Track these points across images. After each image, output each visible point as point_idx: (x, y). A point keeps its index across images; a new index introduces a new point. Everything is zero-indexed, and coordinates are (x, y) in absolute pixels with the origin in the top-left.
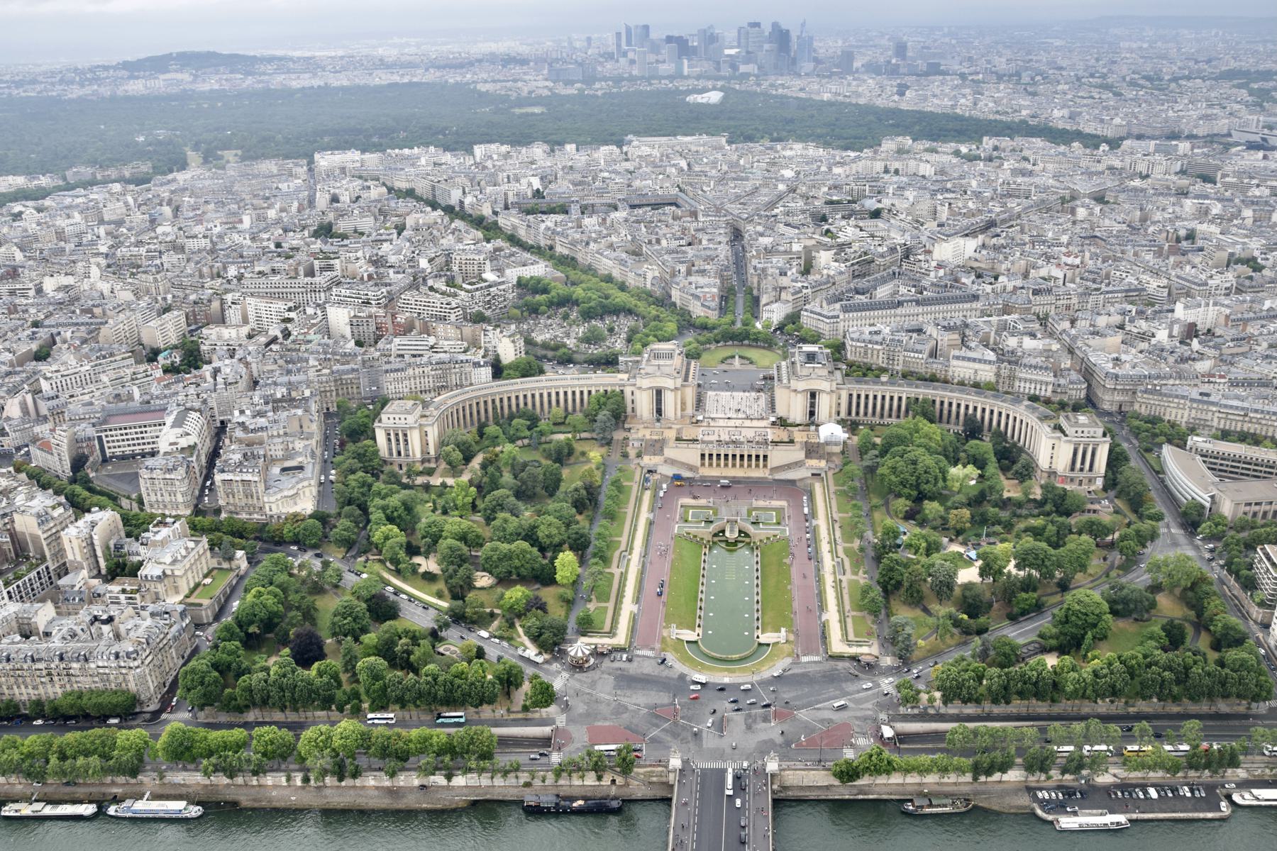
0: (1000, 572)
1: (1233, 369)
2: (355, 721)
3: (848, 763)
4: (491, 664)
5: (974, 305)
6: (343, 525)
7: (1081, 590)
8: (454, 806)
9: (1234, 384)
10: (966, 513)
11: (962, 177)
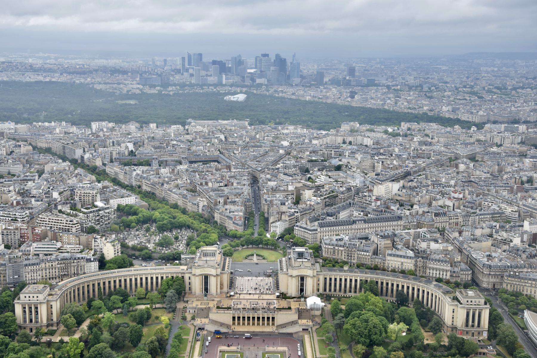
5: (399, 223)
11: (389, 146)
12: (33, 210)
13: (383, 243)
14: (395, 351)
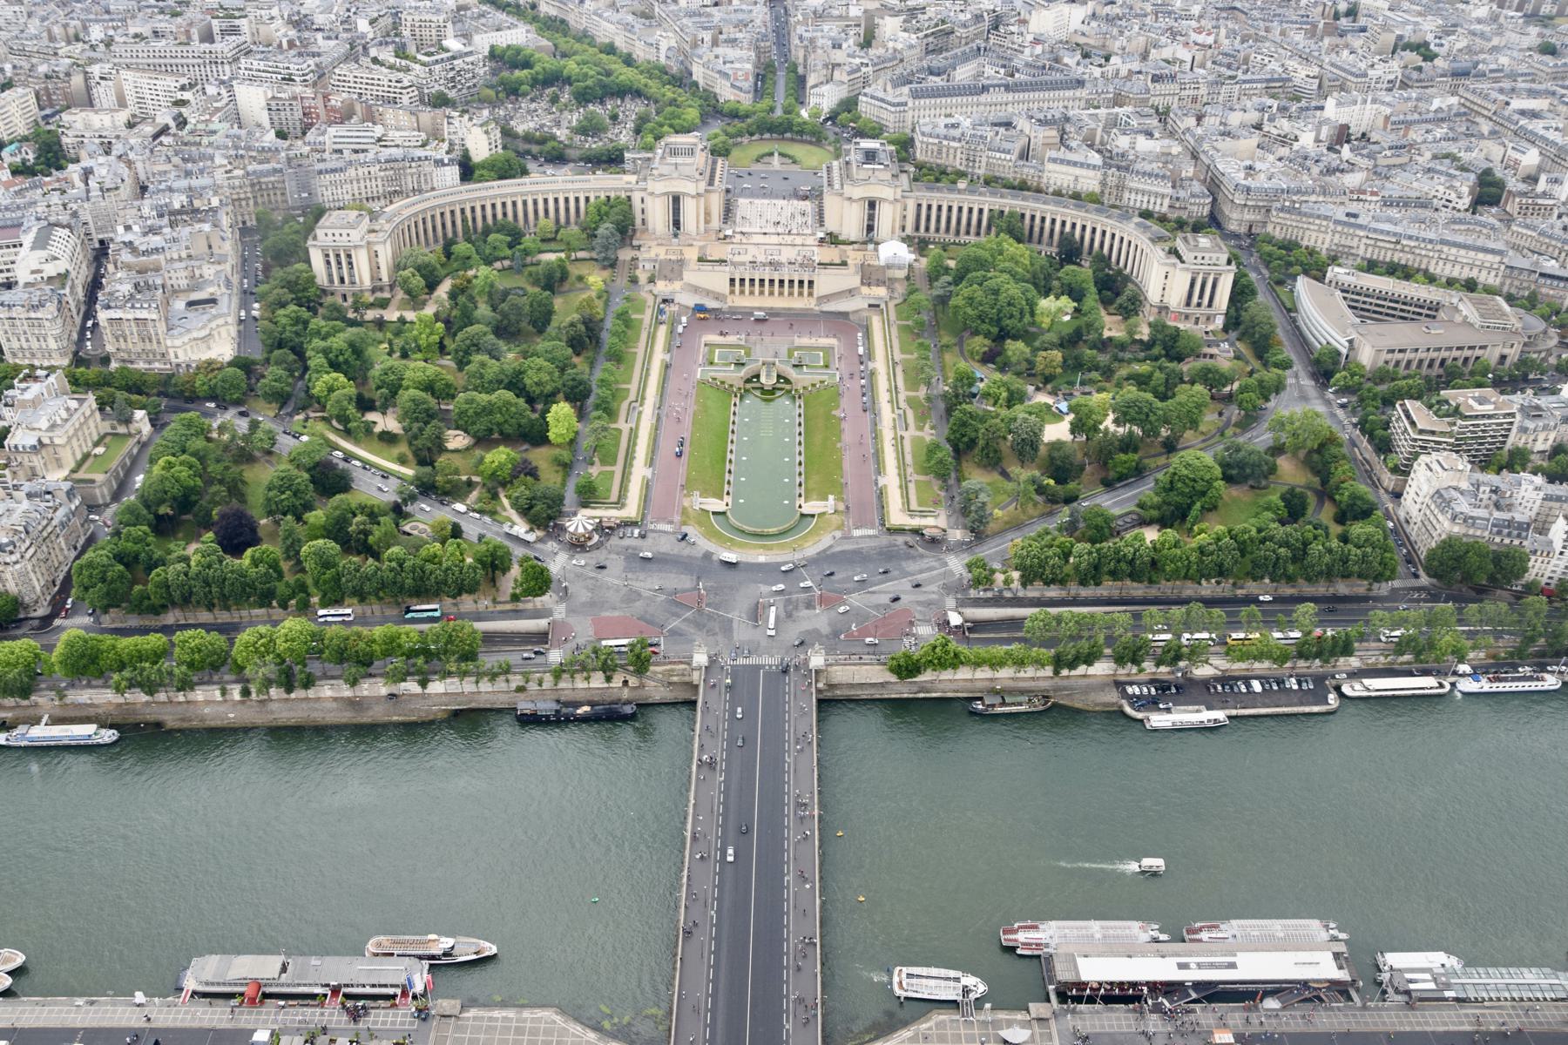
0: (1095, 429)
1: (1388, 184)
2: (303, 619)
3: (907, 656)
4: (471, 544)
5: (1078, 93)
6: (273, 374)
7: (1190, 451)
8: (431, 717)
9: (1388, 203)
10: (1057, 355)
12: (321, 59)
13: (1042, 136)
14: (1046, 350)
